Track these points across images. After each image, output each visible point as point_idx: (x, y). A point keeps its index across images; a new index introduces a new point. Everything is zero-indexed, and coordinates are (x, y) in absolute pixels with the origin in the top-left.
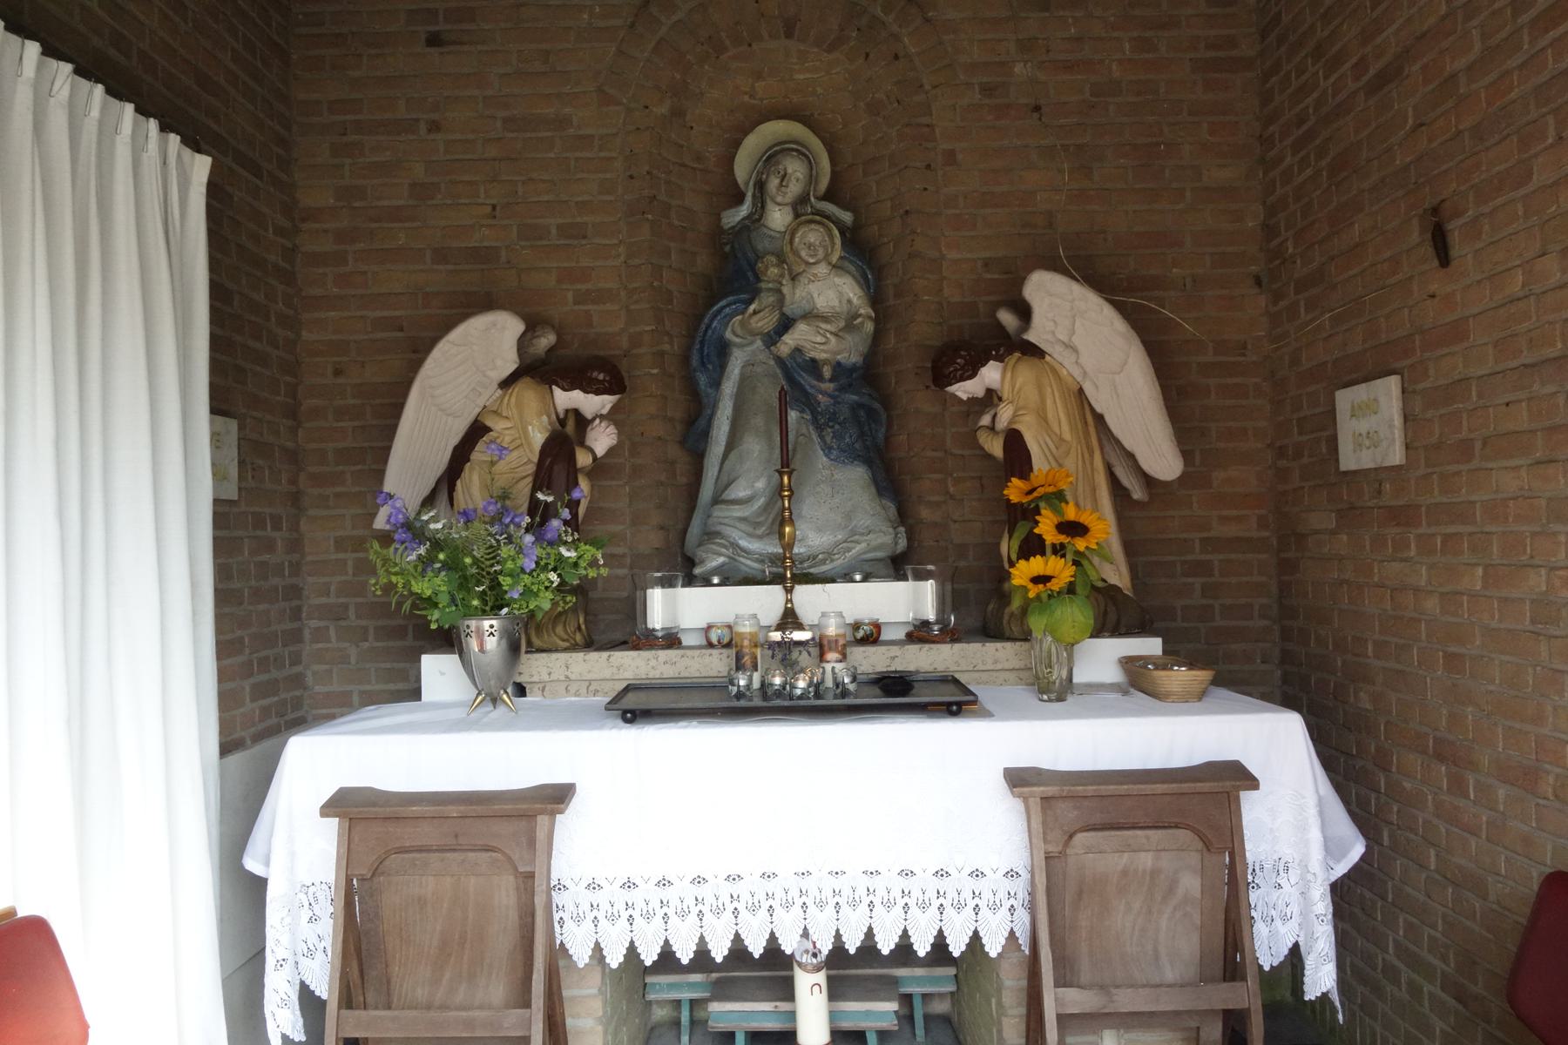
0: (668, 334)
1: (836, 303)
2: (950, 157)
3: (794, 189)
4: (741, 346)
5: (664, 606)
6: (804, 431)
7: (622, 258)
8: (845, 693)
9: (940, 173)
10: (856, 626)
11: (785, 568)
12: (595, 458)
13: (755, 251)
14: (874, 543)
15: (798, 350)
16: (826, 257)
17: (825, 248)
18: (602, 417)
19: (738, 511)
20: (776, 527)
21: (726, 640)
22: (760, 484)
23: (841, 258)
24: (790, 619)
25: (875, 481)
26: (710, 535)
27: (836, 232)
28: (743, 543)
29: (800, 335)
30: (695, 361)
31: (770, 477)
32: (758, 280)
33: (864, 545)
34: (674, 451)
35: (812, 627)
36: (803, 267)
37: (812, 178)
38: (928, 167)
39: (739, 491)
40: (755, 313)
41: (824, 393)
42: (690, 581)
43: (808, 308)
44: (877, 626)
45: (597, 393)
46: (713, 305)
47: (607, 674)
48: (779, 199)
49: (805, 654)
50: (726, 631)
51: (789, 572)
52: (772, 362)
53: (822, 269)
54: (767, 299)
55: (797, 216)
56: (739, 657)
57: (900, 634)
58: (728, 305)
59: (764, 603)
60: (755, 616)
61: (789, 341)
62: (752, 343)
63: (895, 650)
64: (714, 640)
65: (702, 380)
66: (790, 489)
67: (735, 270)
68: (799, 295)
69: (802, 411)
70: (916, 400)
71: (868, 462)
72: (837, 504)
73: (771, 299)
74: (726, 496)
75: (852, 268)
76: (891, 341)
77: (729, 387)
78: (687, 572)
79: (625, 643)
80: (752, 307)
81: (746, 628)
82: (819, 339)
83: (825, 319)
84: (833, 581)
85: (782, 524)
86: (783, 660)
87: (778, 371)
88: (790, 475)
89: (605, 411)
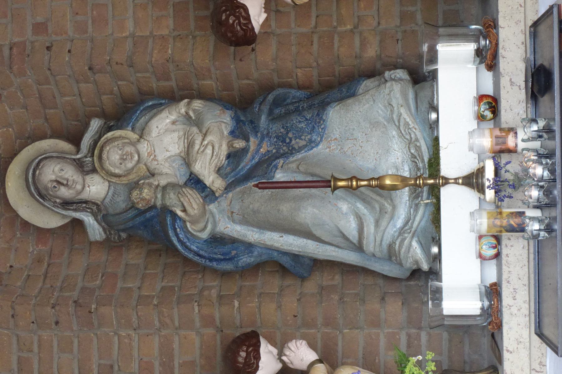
0: (201, 291)
1: (176, 135)
2: (40, 28)
3: (70, 173)
4: (215, 224)
5: (460, 297)
6: (294, 166)
7: (131, 332)
8: (548, 130)
9: (54, 37)
10: (481, 118)
11: (425, 184)
12: (320, 361)
13: (126, 211)
14: (401, 101)
15: (219, 171)
16: (133, 144)
17: (124, 144)
18: (281, 354)
19: (370, 228)
20: (384, 192)
21: (494, 241)
22: (344, 207)
23: (133, 130)
24: (473, 181)
25: (341, 100)
26: (392, 254)
27: (110, 135)
28: (399, 223)
29: (206, 170)
30: (228, 266)
31: (339, 198)
32: (154, 207)
33: (402, 110)
34: (311, 286)
35: (481, 159)
36: (142, 166)
37: (61, 157)
38: (48, 48)
39: (350, 227)
40: (184, 211)
41: (260, 145)
42: (434, 273)
43: (179, 162)
44: (481, 98)
45: (258, 357)
46: (177, 250)
47: (524, 353)
48: (79, 187)
49: (508, 167)
50: (484, 240)
51: (429, 181)
52: (230, 195)
53: (144, 147)
54: (172, 200)
55: (94, 171)
56: (511, 229)
57: (488, 77)
58: (177, 235)
59: (457, 203)
60: (472, 214)
61: (211, 179)
62: (212, 213)
63: (504, 81)
64: (493, 252)
65: (245, 260)
66: (351, 179)
67: (146, 230)
68: (169, 171)
69: (276, 167)
70: (263, 62)
71: (324, 105)
72: (365, 135)
73: (172, 195)
74: (355, 241)
75: (142, 120)
76: (209, 84)
77: (252, 235)
78: (425, 278)
79: (493, 335)
80: (180, 213)
81: (484, 223)
82: (209, 151)
83: (190, 145)
84: (437, 140)
85: (382, 187)
86: (514, 187)
87: (238, 189)
88: (336, 179)
89: (275, 351)
